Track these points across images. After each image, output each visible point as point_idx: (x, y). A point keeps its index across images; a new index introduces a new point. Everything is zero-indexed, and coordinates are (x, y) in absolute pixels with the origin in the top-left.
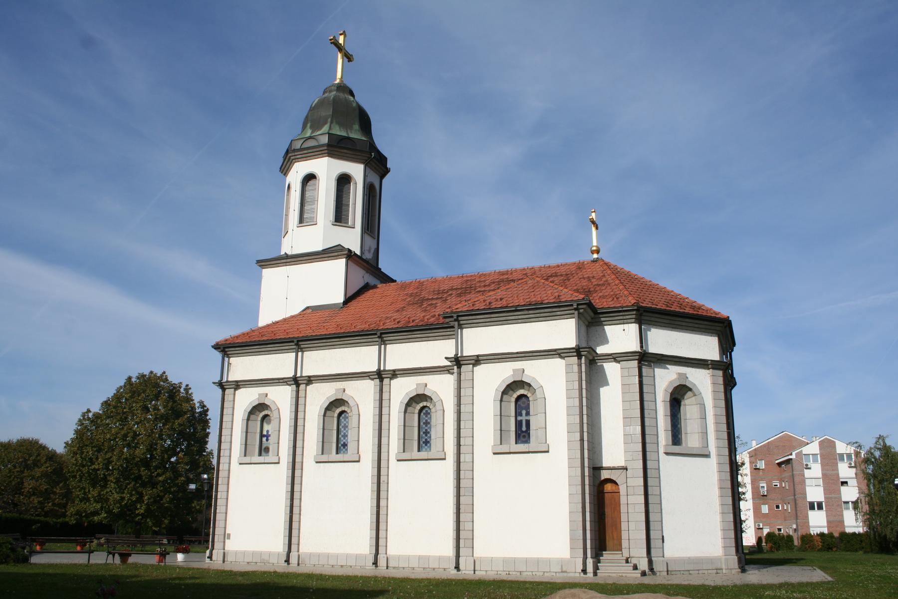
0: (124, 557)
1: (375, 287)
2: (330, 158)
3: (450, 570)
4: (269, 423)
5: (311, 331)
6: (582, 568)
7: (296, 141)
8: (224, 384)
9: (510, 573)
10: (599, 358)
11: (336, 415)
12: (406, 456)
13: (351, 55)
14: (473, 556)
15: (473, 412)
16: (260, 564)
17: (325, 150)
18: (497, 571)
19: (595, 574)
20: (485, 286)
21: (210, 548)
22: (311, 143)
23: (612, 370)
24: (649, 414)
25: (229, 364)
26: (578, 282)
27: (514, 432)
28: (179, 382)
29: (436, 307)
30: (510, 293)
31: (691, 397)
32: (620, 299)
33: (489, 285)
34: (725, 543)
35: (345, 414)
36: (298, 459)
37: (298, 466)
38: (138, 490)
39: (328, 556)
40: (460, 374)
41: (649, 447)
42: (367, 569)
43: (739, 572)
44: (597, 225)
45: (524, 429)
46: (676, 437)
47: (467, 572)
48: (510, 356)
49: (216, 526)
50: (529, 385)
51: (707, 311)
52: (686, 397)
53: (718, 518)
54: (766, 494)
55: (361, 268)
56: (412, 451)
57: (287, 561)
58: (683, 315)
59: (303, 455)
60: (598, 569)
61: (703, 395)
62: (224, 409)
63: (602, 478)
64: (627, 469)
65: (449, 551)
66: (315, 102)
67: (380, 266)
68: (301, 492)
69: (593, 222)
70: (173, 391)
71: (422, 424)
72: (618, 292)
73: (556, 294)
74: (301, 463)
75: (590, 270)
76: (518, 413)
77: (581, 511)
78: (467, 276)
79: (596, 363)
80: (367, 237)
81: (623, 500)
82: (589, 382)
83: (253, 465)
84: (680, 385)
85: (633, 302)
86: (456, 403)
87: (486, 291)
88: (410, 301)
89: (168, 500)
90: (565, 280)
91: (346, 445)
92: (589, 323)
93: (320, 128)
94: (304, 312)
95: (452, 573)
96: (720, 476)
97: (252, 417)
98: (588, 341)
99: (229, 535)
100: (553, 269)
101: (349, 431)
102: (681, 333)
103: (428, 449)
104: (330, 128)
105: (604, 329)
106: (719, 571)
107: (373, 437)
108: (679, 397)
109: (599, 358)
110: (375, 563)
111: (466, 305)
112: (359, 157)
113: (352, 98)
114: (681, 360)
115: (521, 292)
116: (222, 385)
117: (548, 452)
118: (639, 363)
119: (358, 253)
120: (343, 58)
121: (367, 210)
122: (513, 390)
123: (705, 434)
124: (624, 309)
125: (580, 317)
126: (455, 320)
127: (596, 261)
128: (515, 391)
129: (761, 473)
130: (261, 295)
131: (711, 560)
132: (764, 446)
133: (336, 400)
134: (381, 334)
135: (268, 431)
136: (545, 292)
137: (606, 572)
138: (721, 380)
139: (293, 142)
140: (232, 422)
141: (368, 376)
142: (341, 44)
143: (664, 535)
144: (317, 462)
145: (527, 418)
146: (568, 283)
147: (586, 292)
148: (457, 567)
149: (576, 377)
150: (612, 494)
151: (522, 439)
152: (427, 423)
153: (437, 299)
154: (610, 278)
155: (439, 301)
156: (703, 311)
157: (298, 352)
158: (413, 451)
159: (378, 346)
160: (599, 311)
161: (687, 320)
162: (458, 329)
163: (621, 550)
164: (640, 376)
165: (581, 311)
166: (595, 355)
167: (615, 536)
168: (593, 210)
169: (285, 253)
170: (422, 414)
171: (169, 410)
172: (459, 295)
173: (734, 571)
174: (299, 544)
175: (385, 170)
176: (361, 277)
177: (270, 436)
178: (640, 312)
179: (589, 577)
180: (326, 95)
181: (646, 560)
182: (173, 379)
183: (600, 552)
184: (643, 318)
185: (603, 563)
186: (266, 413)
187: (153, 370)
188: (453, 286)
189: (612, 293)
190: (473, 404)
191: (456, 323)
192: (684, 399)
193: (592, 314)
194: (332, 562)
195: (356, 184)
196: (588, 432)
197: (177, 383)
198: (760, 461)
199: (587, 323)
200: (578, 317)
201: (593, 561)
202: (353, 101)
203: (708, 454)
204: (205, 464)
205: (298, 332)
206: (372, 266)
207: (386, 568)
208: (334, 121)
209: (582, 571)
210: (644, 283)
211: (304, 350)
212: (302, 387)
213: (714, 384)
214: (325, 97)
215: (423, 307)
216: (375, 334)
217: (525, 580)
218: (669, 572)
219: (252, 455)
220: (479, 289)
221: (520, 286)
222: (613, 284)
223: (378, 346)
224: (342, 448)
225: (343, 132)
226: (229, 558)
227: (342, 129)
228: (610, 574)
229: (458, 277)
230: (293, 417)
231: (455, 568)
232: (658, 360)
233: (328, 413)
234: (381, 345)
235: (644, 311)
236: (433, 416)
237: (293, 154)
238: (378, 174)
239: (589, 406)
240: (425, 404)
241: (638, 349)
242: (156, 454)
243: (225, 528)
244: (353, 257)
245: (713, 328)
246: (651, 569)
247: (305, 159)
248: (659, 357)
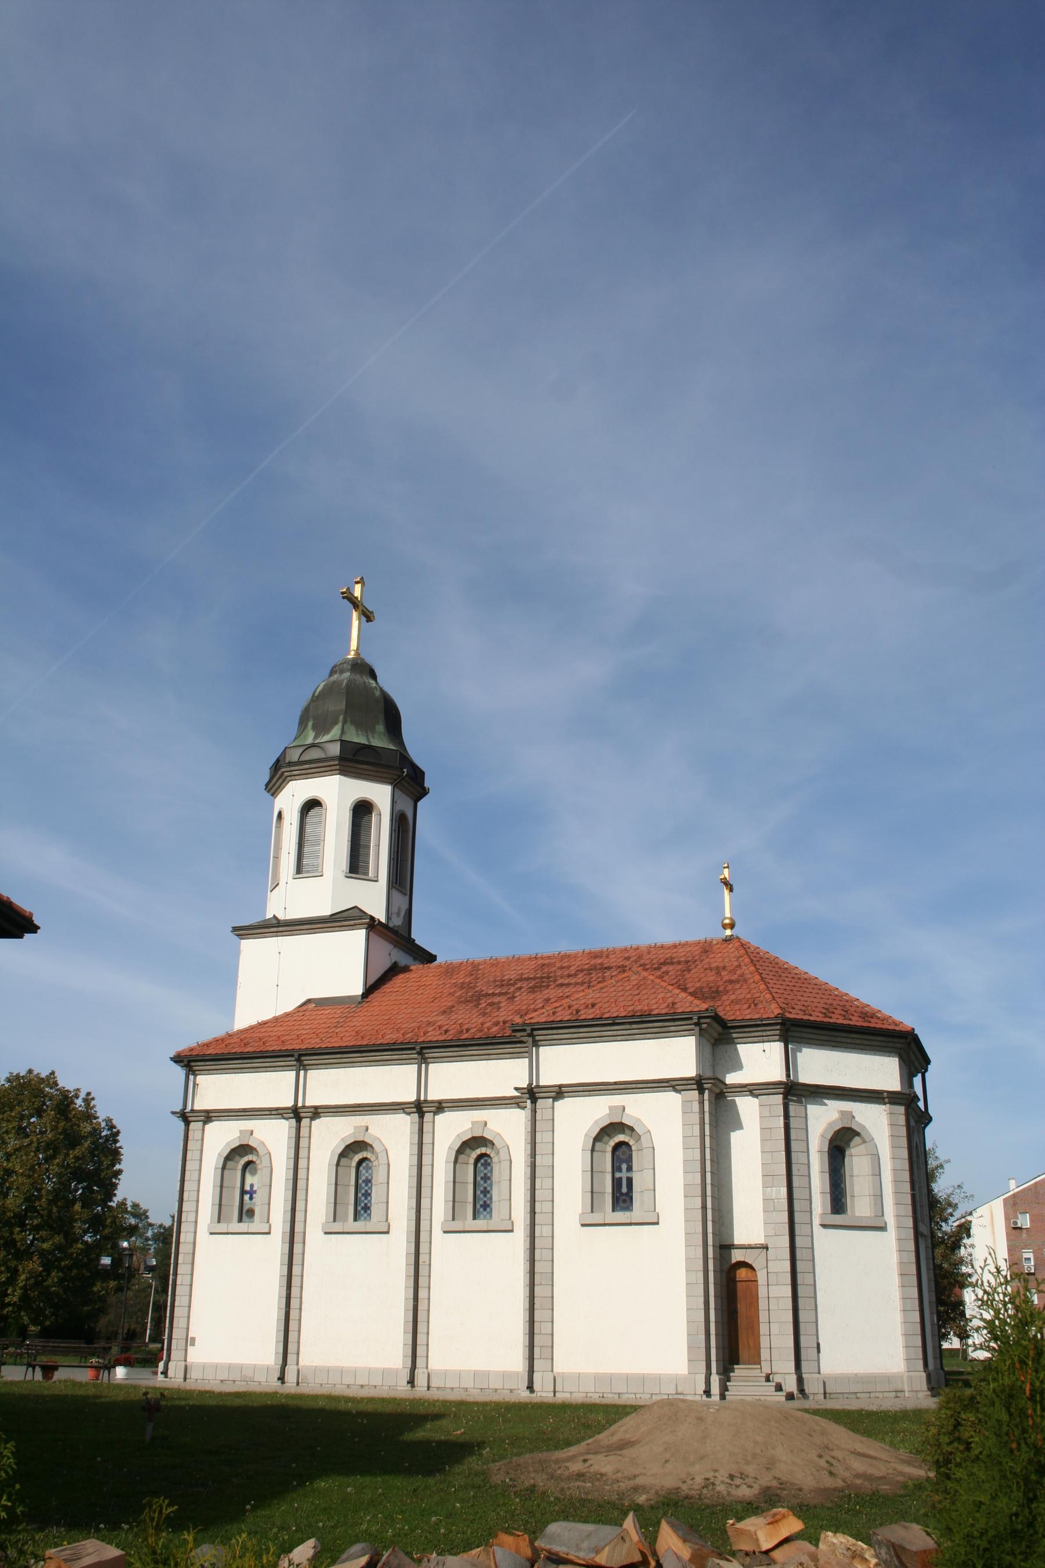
0: (48, 1370)
1: (406, 969)
2: (342, 777)
3: (520, 1391)
4: (254, 1173)
5: (318, 1040)
6: (704, 1389)
7: (292, 749)
8: (188, 1115)
9: (605, 1395)
10: (729, 1090)
11: (354, 1164)
12: (457, 1225)
14: (552, 1371)
15: (553, 1166)
16: (239, 1383)
17: (336, 765)
18: (587, 1393)
19: (723, 1397)
20: (569, 976)
21: (164, 1358)
22: (314, 754)
23: (747, 1107)
24: (798, 1170)
25: (195, 1084)
26: (703, 975)
27: (611, 1195)
28: (76, 1087)
29: (500, 1008)
30: (605, 995)
32: (760, 1006)
33: (575, 975)
34: (907, 1353)
35: (367, 1162)
36: (298, 1228)
37: (298, 1238)
38: (9, 1264)
39: (342, 1371)
40: (534, 1111)
41: (798, 1217)
42: (402, 1389)
43: (928, 1395)
44: (731, 886)
45: (624, 1190)
46: (838, 1201)
47: (544, 1394)
48: (606, 1087)
49: (174, 1326)
50: (632, 1129)
51: (883, 1020)
52: (852, 1144)
53: (898, 1317)
54: (1033, 1271)
55: (387, 940)
56: (465, 1219)
57: (282, 1379)
59: (305, 1221)
60: (727, 1390)
61: (877, 1141)
62: (188, 1152)
63: (734, 1261)
64: (767, 1248)
65: (517, 1363)
66: (320, 688)
67: (413, 936)
68: (302, 1276)
69: (726, 883)
70: (65, 1100)
71: (478, 1179)
72: (757, 995)
73: (670, 1000)
74: (302, 1235)
75: (720, 955)
76: (616, 1168)
77: (703, 1307)
78: (542, 958)
79: (726, 1097)
80: (395, 894)
81: (762, 1292)
82: (715, 1124)
84: (843, 1128)
85: (777, 1011)
86: (529, 1153)
87: (571, 984)
88: (460, 997)
89: (56, 1280)
90: (684, 971)
91: (369, 1208)
92: (716, 1040)
93: (327, 731)
94: (304, 1008)
95: (524, 1395)
96: (900, 1257)
97: (230, 1164)
98: (714, 1066)
99: (193, 1339)
100: (667, 951)
101: (374, 1188)
102: (845, 1053)
103: (488, 1216)
104: (343, 732)
105: (736, 1049)
106: (899, 1394)
107: (409, 1198)
108: (842, 1144)
109: (729, 1090)
110: (411, 1382)
111: (543, 1013)
112: (385, 775)
113: (372, 682)
114: (846, 1093)
115: (620, 994)
116: (185, 1117)
117: (657, 1223)
118: (785, 1098)
119: (383, 920)
120: (359, 619)
121: (396, 854)
123: (879, 1197)
124: (764, 1022)
125: (702, 1034)
126: (529, 1035)
127: (730, 940)
129: (1024, 1235)
130: (239, 979)
131: (888, 1378)
132: (1029, 1189)
133: (355, 1142)
134: (422, 1048)
135: (252, 1186)
136: (654, 995)
137: (738, 1393)
138: (902, 1120)
139: (287, 750)
140: (200, 1170)
141: (403, 1109)
142: (356, 598)
143: (820, 1341)
144: (326, 1233)
145: (629, 1175)
146: (688, 976)
147: (713, 991)
148: (530, 1388)
149: (696, 1118)
150: (748, 1283)
151: (621, 1204)
152: (486, 1178)
153: (500, 994)
154: (748, 970)
155: (503, 999)
156: (877, 1021)
157: (300, 1070)
158: (466, 1219)
159: (416, 1065)
160: (729, 1025)
161: (853, 1036)
162: (533, 1046)
163: (760, 1363)
164: (787, 1116)
165: (704, 1026)
166: (722, 1086)
167: (752, 1345)
168: (726, 865)
169: (274, 916)
170: (479, 1165)
171: (60, 1134)
172: (532, 990)
173: (921, 1395)
174: (298, 1354)
175: (420, 789)
176: (388, 954)
177: (255, 1192)
178: (786, 1027)
179: (714, 1401)
180: (335, 677)
181: (794, 1377)
182: (66, 1082)
183: (730, 1366)
184: (790, 1034)
185: (735, 1381)
186: (250, 1159)
187: (32, 1068)
188: (522, 974)
189: (749, 996)
190: (553, 1154)
191: (530, 1039)
193: (720, 1029)
194: (347, 1380)
195: (380, 815)
196: (713, 1197)
197: (72, 1090)
198: (1023, 1215)
199: (713, 1041)
200: (700, 1035)
201: (720, 1379)
202: (376, 687)
203: (883, 1225)
204: (114, 1222)
205: (299, 1041)
206: (401, 936)
207: (426, 1389)
209: (705, 1392)
210: (795, 976)
211: (307, 1067)
212: (305, 1122)
213: (892, 1125)
214: (334, 682)
215: (481, 1006)
216: (414, 1049)
217: (626, 1404)
218: (828, 1395)
219: (229, 1221)
220: (560, 981)
221: (619, 984)
222: (752, 981)
223: (416, 1065)
224: (362, 1212)
225: (361, 736)
226: (193, 1375)
227: (359, 733)
228: (743, 1397)
229: (530, 959)
230: (292, 1166)
231: (528, 1388)
232: (812, 1092)
233: (343, 1161)
234: (422, 1063)
235: (792, 1025)
236: (496, 1168)
237: (288, 769)
238: (411, 798)
239: (715, 1160)
240: (483, 1150)
241: (784, 1079)
242: (41, 1206)
243: (188, 1329)
244: (378, 927)
245: (890, 1045)
246: (802, 1390)
248: (812, 1089)
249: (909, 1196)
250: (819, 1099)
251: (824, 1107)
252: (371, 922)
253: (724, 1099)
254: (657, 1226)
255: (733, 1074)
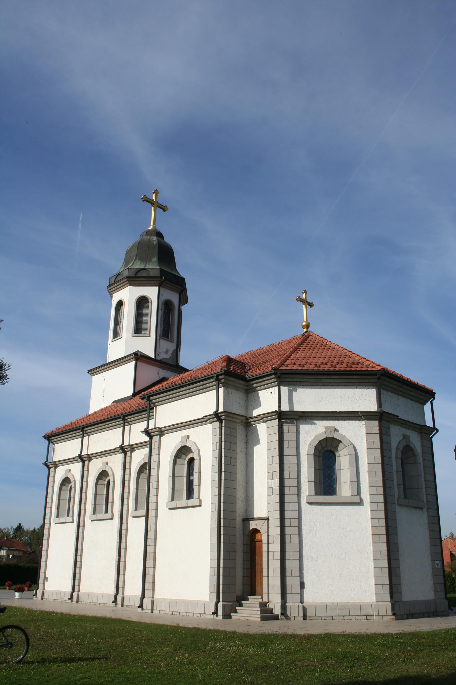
2: (131, 287)
10: (253, 420)
13: (165, 207)
17: (126, 281)
24: (289, 467)
31: (344, 449)
43: (393, 619)
58: (313, 372)
79: (252, 425)
83: (61, 524)
92: (247, 390)
99: (47, 578)
108: (332, 449)
109: (253, 420)
114: (327, 415)
122: (185, 454)
128: (187, 454)
143: (305, 580)
161: (333, 377)
192: (338, 450)
208: (138, 258)
232: (300, 416)
238: (178, 293)
244: (141, 358)
245: (366, 381)
247: (117, 290)
248: (300, 414)
249: (381, 481)
250: (309, 421)
251: (313, 426)
252: (136, 357)
253: (251, 426)
254: (200, 508)
255: (256, 410)
